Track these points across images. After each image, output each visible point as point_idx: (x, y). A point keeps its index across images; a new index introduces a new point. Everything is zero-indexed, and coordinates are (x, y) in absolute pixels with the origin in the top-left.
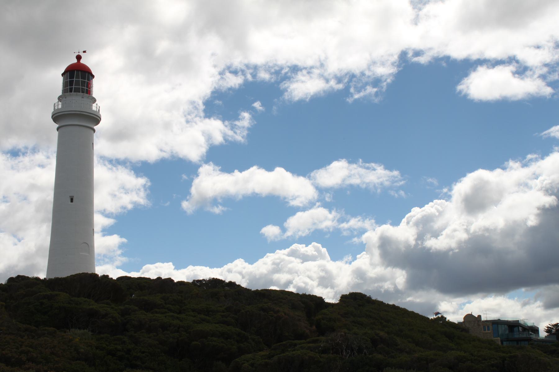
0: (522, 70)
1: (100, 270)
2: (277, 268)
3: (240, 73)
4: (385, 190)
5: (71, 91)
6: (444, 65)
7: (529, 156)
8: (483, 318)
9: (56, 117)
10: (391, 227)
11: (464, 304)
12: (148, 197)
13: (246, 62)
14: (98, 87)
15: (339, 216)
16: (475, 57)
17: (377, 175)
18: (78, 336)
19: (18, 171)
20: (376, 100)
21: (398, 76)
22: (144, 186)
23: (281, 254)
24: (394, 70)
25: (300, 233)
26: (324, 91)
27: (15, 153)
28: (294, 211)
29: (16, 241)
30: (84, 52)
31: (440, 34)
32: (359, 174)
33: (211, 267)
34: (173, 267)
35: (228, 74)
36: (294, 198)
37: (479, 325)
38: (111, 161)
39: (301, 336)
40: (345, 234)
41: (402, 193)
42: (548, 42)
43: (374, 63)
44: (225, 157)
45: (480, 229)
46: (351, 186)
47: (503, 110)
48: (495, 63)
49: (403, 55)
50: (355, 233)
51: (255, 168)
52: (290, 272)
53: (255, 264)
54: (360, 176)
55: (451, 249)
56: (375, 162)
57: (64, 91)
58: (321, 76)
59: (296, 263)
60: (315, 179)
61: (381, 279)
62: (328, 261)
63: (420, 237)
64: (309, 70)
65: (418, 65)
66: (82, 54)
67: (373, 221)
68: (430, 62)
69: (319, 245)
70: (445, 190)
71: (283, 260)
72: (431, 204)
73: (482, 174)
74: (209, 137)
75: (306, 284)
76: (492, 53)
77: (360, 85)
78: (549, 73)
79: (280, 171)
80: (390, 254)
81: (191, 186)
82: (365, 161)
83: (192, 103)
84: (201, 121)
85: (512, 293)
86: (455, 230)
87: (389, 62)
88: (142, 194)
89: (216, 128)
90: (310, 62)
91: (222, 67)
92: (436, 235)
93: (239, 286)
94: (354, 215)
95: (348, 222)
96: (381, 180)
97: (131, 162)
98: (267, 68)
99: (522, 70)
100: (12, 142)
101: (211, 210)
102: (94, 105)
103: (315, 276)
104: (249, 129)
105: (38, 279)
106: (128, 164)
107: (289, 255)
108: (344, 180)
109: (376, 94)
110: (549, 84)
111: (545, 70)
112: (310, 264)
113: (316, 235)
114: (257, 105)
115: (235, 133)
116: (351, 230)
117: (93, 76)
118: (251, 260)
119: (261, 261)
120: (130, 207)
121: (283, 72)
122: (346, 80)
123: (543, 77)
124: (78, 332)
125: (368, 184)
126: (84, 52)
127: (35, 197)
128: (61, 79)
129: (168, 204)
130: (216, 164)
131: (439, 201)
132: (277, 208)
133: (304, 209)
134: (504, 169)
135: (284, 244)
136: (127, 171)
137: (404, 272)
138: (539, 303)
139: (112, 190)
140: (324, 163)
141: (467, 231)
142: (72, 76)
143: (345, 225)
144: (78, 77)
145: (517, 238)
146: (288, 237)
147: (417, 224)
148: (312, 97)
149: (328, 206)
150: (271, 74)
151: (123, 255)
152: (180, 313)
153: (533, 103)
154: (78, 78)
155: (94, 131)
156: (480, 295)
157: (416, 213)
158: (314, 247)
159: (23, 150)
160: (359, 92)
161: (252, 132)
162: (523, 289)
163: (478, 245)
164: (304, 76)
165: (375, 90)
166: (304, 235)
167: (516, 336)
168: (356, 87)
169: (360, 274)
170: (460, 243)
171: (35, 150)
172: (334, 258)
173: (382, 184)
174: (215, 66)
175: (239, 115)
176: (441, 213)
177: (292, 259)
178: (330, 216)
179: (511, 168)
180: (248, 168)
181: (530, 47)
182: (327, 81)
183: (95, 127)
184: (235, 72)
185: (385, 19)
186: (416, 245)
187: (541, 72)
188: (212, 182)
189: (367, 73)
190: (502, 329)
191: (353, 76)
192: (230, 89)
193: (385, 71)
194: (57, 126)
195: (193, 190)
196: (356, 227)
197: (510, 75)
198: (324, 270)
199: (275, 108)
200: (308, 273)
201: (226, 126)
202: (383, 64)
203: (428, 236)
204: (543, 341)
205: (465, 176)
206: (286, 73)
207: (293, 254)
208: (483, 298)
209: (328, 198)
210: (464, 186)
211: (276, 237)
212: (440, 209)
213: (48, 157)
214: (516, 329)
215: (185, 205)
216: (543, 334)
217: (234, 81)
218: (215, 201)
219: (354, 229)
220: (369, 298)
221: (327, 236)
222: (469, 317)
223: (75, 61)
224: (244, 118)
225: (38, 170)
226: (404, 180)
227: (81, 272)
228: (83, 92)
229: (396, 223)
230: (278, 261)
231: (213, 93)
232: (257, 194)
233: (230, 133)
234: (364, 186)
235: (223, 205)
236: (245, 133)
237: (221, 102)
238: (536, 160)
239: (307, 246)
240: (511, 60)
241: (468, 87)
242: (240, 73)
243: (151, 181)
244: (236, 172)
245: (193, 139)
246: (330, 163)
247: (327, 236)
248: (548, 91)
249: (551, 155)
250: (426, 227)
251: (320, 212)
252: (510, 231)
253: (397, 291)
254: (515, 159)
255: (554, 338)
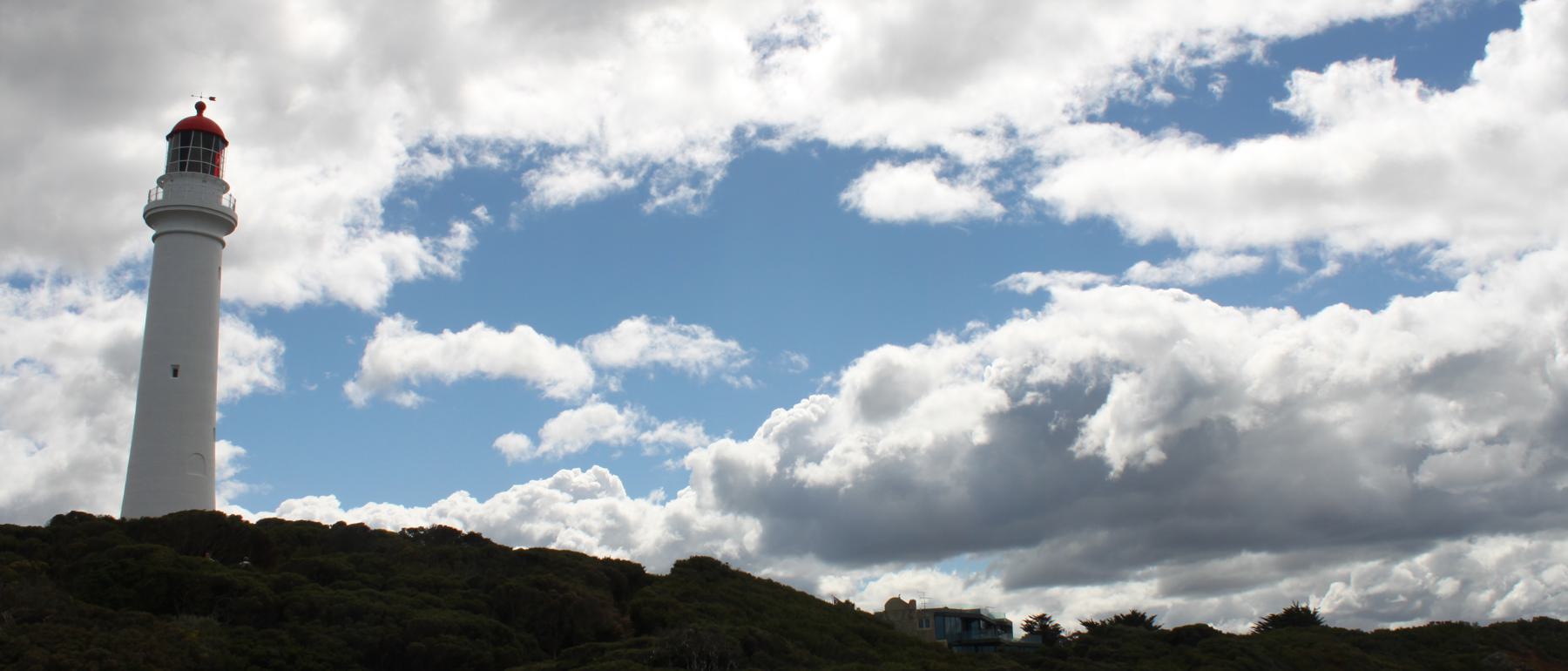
0: (953, 171)
1: (224, 505)
2: (529, 510)
3: (446, 154)
4: (716, 374)
5: (182, 168)
6: (815, 155)
7: (971, 325)
9: (153, 216)
13: (459, 133)
14: (234, 164)
15: (636, 417)
16: (871, 144)
17: (699, 349)
18: (193, 628)
19: (29, 318)
20: (695, 210)
21: (732, 167)
22: (275, 352)
23: (540, 486)
24: (726, 157)
25: (567, 447)
26: (601, 191)
27: (22, 282)
28: (556, 407)
30: (212, 99)
31: (806, 99)
32: (669, 342)
33: (409, 504)
34: (338, 503)
35: (427, 156)
36: (555, 383)
37: (911, 618)
39: (608, 635)
40: (649, 452)
41: (747, 380)
42: (996, 124)
43: (692, 143)
44: (424, 303)
46: (656, 364)
47: (917, 238)
48: (902, 157)
49: (739, 133)
50: (668, 451)
51: (480, 325)
52: (553, 518)
53: (488, 503)
54: (673, 348)
55: (840, 483)
56: (700, 323)
57: (170, 168)
58: (593, 164)
59: (563, 504)
60: (591, 349)
61: (718, 534)
63: (786, 461)
65: (770, 153)
67: (701, 429)
68: (790, 149)
70: (827, 379)
71: (537, 496)
72: (804, 402)
73: (890, 353)
74: (393, 265)
75: (578, 542)
76: (901, 139)
77: (667, 181)
78: (999, 178)
79: (524, 332)
80: (733, 490)
81: (363, 354)
82: (680, 321)
83: (361, 203)
84: (380, 237)
85: (946, 562)
86: (848, 450)
87: (717, 142)
88: (270, 366)
89: (410, 251)
90: (572, 138)
91: (413, 141)
92: (816, 456)
93: (488, 541)
94: (664, 418)
95: (653, 429)
98: (496, 146)
99: (953, 171)
102: (225, 197)
103: (596, 525)
104: (466, 253)
105: (109, 519)
106: (243, 312)
107: (551, 487)
108: (642, 354)
109: (696, 199)
111: (993, 172)
113: (595, 453)
114: (480, 212)
115: (440, 259)
117: (226, 143)
119: (499, 497)
120: (247, 389)
121: (525, 154)
122: (641, 175)
123: (988, 185)
125: (683, 361)
126: (212, 99)
127: (66, 367)
128: (164, 146)
131: (818, 397)
132: (521, 401)
133: (573, 405)
134: (929, 344)
135: (542, 467)
136: (242, 324)
138: (995, 581)
139: (241, 361)
140: (606, 323)
141: (869, 451)
142: (185, 141)
143: (648, 437)
144: (196, 143)
145: (958, 464)
146: (545, 454)
147: (779, 439)
148: (579, 199)
149: (610, 398)
150: (503, 157)
151: (237, 477)
152: (383, 588)
154: (197, 144)
155: (223, 244)
156: (891, 565)
157: (780, 418)
158: (596, 473)
159: (37, 276)
160: (665, 194)
161: (472, 259)
162: (967, 556)
163: (890, 479)
164: (563, 162)
165: (694, 192)
166: (574, 450)
167: (975, 636)
168: (659, 187)
169: (679, 524)
170: (856, 472)
171: (61, 280)
172: (635, 491)
173: (709, 363)
175: (450, 227)
176: (823, 419)
177: (556, 493)
178: (620, 418)
179: (941, 344)
180: (468, 326)
181: (965, 131)
182: (607, 173)
183: (226, 238)
184: (436, 151)
185: (702, 67)
186: (777, 477)
187: (985, 176)
188: (399, 349)
189: (679, 159)
190: (951, 625)
192: (430, 179)
193: (710, 157)
194: (152, 232)
195: (366, 362)
196: (670, 440)
197: (932, 178)
198: (612, 514)
199: (513, 216)
200: (584, 521)
201: (425, 247)
202: (705, 144)
203: (800, 461)
204: (1019, 645)
205: (861, 355)
206: (531, 157)
207: (560, 485)
208: (896, 571)
209: (614, 385)
210: (859, 373)
211: (522, 453)
213: (88, 293)
214: (974, 625)
215: (350, 388)
216: (1019, 633)
217: (437, 167)
218: (405, 384)
219: (667, 445)
220: (726, 567)
221: (618, 454)
222: (895, 604)
223: (194, 113)
224: (457, 234)
225: (70, 318)
228: (205, 171)
230: (529, 497)
231: (397, 185)
232: (484, 374)
233: (432, 260)
235: (420, 391)
236: (459, 260)
237: (414, 203)
238: (983, 331)
239: (584, 471)
240: (931, 152)
241: (860, 196)
242: (446, 154)
243: (287, 345)
244: (447, 334)
245: (367, 267)
246: (616, 324)
247: (618, 454)
248: (997, 209)
250: (797, 445)
251: (600, 412)
252: (943, 453)
253: (744, 555)
254: (946, 330)
255: (1038, 641)
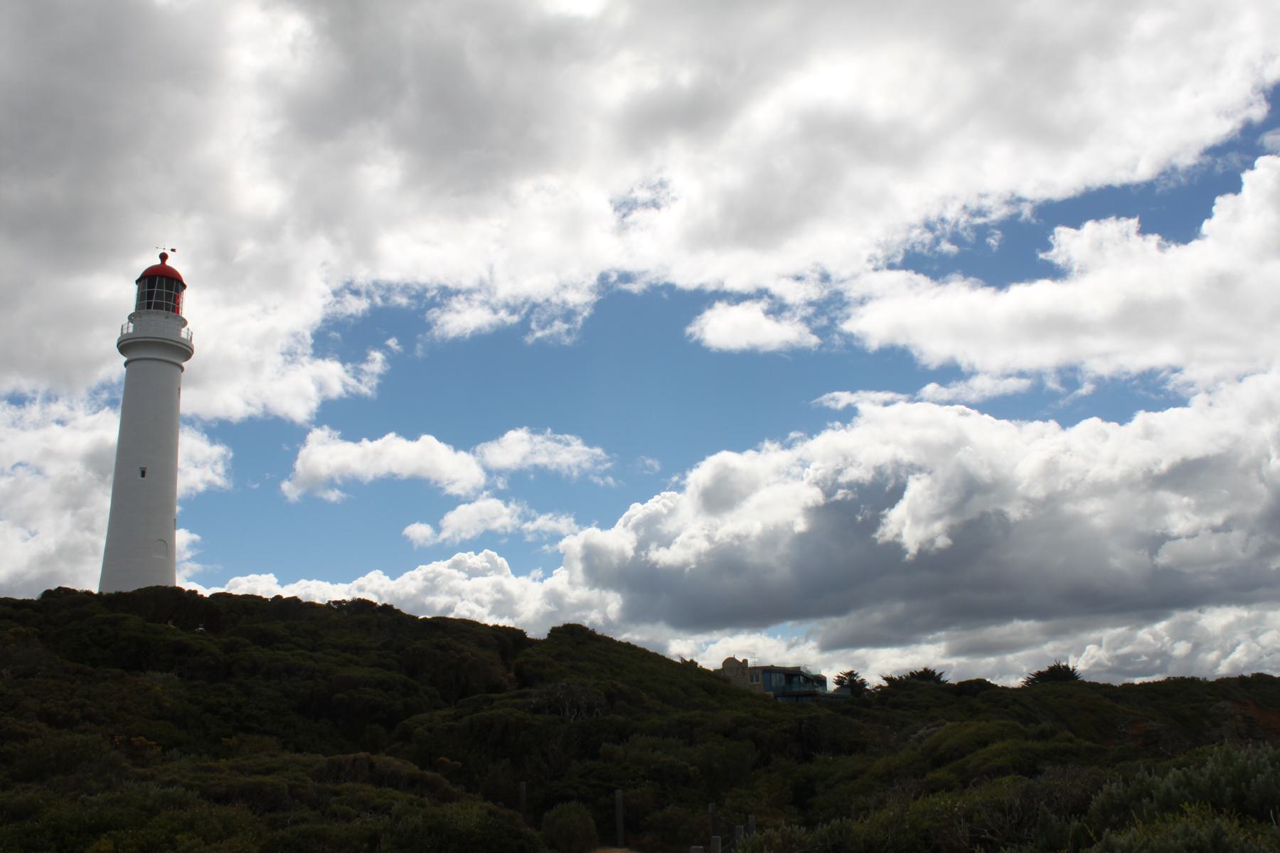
0: (778, 309)
2: (432, 586)
3: (364, 295)
4: (585, 475)
5: (149, 307)
6: (665, 296)
7: (793, 435)
8: (750, 663)
10: (597, 531)
11: (707, 644)
12: (228, 473)
13: (375, 277)
14: (191, 304)
15: (519, 510)
16: (711, 287)
17: (570, 454)
18: (160, 683)
19: (23, 429)
20: (567, 341)
21: (598, 306)
22: (224, 457)
23: (441, 566)
25: (463, 535)
26: (491, 325)
27: (18, 400)
28: (454, 502)
29: (26, 533)
30: (173, 250)
32: (546, 449)
36: (453, 483)
38: (1245, 376)
39: (497, 688)
40: (529, 538)
41: (610, 480)
42: (813, 271)
43: (565, 287)
44: (346, 417)
45: (728, 536)
46: (536, 466)
47: (749, 364)
48: (737, 298)
49: (603, 278)
50: (545, 538)
51: (392, 435)
52: (452, 592)
53: (398, 580)
54: (550, 453)
55: (686, 564)
56: (571, 433)
57: (138, 307)
58: (484, 303)
59: (460, 581)
61: (586, 605)
62: (507, 576)
63: (642, 546)
64: (469, 292)
65: (628, 294)
66: (168, 252)
67: (572, 520)
68: (645, 291)
69: (494, 554)
70: (675, 479)
72: (657, 497)
73: (726, 458)
74: (321, 386)
75: (472, 612)
76: (736, 284)
77: (544, 317)
78: (815, 315)
79: (428, 440)
80: (599, 569)
81: (296, 459)
82: (555, 431)
83: (294, 335)
84: (310, 363)
85: (773, 628)
86: (692, 537)
87: (585, 286)
88: (220, 468)
89: (334, 375)
90: (467, 283)
91: (337, 284)
92: (666, 542)
93: (398, 611)
95: (533, 520)
96: (578, 459)
97: (202, 421)
98: (405, 289)
99: (778, 309)
100: (25, 385)
101: (325, 496)
102: (184, 330)
103: (486, 598)
104: (380, 376)
105: (89, 593)
106: (198, 424)
108: (524, 458)
109: (569, 332)
110: (815, 331)
111: (810, 310)
112: (478, 581)
113: (485, 540)
114: (392, 342)
115: (359, 381)
116: (537, 532)
118: (394, 574)
119: (407, 575)
120: (201, 487)
121: (429, 295)
122: (523, 312)
123: (807, 320)
124: (158, 675)
126: (173, 250)
127: (54, 469)
128: (134, 289)
129: (256, 486)
130: (334, 427)
131: (668, 494)
132: (426, 497)
133: (468, 500)
134: (758, 450)
135: (442, 551)
136: (197, 434)
137: (619, 596)
140: (495, 433)
141: (709, 538)
142: (151, 285)
143: (529, 526)
144: (160, 286)
146: (444, 540)
147: (636, 528)
148: (472, 332)
149: (502, 496)
150: (411, 297)
151: (194, 559)
152: (313, 650)
153: (791, 358)
154: (161, 287)
155: (182, 369)
156: (727, 631)
157: (637, 511)
158: (486, 555)
159: (30, 395)
160: (543, 328)
161: (385, 382)
162: (789, 624)
163: (726, 560)
164: (459, 302)
165: (566, 326)
166: (468, 537)
167: (796, 689)
168: (538, 321)
169: (554, 597)
170: (699, 555)
171: (50, 398)
172: (517, 571)
173: (579, 466)
174: (327, 282)
175: (367, 355)
176: (672, 512)
177: (454, 572)
178: (506, 511)
179: (768, 450)
180: (382, 435)
181: (787, 277)
182: (495, 311)
183: (184, 364)
184: (356, 293)
187: (804, 313)
188: (326, 454)
189: (554, 299)
190: (776, 680)
191: (535, 306)
192: (351, 316)
193: (579, 298)
194: (124, 359)
195: (299, 465)
197: (761, 315)
198: (499, 589)
199: (419, 346)
200: (477, 595)
201: (347, 371)
202: (576, 287)
203: (653, 546)
205: (703, 459)
206: (433, 298)
207: (457, 566)
208: (731, 636)
209: (501, 484)
210: (702, 474)
211: (426, 540)
212: (671, 505)
213: (71, 409)
214: (795, 679)
215: (286, 486)
216: (832, 687)
217: (357, 306)
218: (330, 483)
219: (545, 533)
220: (593, 632)
221: (504, 541)
222: (730, 663)
223: (158, 262)
224: (374, 360)
225: (56, 429)
226: (610, 461)
227: (154, 585)
229: (607, 524)
230: (432, 575)
231: (324, 321)
232: (395, 475)
233: (352, 382)
234: (554, 467)
236: (375, 382)
237: (338, 335)
238: (803, 440)
239: (477, 554)
240: (761, 294)
241: (702, 329)
242: (364, 295)
244: (365, 442)
245: (300, 388)
246: (502, 433)
247: (504, 541)
248: (814, 340)
249: (1004, 422)
250: (651, 533)
251: (494, 505)
252: (770, 539)
255: (847, 693)
